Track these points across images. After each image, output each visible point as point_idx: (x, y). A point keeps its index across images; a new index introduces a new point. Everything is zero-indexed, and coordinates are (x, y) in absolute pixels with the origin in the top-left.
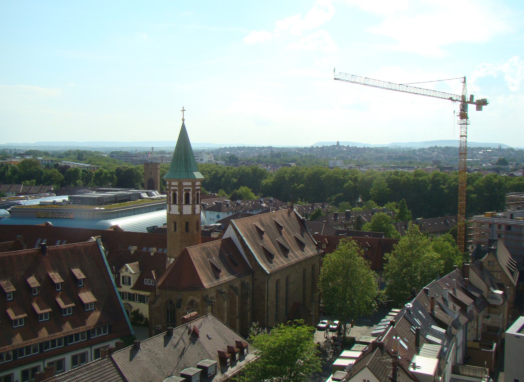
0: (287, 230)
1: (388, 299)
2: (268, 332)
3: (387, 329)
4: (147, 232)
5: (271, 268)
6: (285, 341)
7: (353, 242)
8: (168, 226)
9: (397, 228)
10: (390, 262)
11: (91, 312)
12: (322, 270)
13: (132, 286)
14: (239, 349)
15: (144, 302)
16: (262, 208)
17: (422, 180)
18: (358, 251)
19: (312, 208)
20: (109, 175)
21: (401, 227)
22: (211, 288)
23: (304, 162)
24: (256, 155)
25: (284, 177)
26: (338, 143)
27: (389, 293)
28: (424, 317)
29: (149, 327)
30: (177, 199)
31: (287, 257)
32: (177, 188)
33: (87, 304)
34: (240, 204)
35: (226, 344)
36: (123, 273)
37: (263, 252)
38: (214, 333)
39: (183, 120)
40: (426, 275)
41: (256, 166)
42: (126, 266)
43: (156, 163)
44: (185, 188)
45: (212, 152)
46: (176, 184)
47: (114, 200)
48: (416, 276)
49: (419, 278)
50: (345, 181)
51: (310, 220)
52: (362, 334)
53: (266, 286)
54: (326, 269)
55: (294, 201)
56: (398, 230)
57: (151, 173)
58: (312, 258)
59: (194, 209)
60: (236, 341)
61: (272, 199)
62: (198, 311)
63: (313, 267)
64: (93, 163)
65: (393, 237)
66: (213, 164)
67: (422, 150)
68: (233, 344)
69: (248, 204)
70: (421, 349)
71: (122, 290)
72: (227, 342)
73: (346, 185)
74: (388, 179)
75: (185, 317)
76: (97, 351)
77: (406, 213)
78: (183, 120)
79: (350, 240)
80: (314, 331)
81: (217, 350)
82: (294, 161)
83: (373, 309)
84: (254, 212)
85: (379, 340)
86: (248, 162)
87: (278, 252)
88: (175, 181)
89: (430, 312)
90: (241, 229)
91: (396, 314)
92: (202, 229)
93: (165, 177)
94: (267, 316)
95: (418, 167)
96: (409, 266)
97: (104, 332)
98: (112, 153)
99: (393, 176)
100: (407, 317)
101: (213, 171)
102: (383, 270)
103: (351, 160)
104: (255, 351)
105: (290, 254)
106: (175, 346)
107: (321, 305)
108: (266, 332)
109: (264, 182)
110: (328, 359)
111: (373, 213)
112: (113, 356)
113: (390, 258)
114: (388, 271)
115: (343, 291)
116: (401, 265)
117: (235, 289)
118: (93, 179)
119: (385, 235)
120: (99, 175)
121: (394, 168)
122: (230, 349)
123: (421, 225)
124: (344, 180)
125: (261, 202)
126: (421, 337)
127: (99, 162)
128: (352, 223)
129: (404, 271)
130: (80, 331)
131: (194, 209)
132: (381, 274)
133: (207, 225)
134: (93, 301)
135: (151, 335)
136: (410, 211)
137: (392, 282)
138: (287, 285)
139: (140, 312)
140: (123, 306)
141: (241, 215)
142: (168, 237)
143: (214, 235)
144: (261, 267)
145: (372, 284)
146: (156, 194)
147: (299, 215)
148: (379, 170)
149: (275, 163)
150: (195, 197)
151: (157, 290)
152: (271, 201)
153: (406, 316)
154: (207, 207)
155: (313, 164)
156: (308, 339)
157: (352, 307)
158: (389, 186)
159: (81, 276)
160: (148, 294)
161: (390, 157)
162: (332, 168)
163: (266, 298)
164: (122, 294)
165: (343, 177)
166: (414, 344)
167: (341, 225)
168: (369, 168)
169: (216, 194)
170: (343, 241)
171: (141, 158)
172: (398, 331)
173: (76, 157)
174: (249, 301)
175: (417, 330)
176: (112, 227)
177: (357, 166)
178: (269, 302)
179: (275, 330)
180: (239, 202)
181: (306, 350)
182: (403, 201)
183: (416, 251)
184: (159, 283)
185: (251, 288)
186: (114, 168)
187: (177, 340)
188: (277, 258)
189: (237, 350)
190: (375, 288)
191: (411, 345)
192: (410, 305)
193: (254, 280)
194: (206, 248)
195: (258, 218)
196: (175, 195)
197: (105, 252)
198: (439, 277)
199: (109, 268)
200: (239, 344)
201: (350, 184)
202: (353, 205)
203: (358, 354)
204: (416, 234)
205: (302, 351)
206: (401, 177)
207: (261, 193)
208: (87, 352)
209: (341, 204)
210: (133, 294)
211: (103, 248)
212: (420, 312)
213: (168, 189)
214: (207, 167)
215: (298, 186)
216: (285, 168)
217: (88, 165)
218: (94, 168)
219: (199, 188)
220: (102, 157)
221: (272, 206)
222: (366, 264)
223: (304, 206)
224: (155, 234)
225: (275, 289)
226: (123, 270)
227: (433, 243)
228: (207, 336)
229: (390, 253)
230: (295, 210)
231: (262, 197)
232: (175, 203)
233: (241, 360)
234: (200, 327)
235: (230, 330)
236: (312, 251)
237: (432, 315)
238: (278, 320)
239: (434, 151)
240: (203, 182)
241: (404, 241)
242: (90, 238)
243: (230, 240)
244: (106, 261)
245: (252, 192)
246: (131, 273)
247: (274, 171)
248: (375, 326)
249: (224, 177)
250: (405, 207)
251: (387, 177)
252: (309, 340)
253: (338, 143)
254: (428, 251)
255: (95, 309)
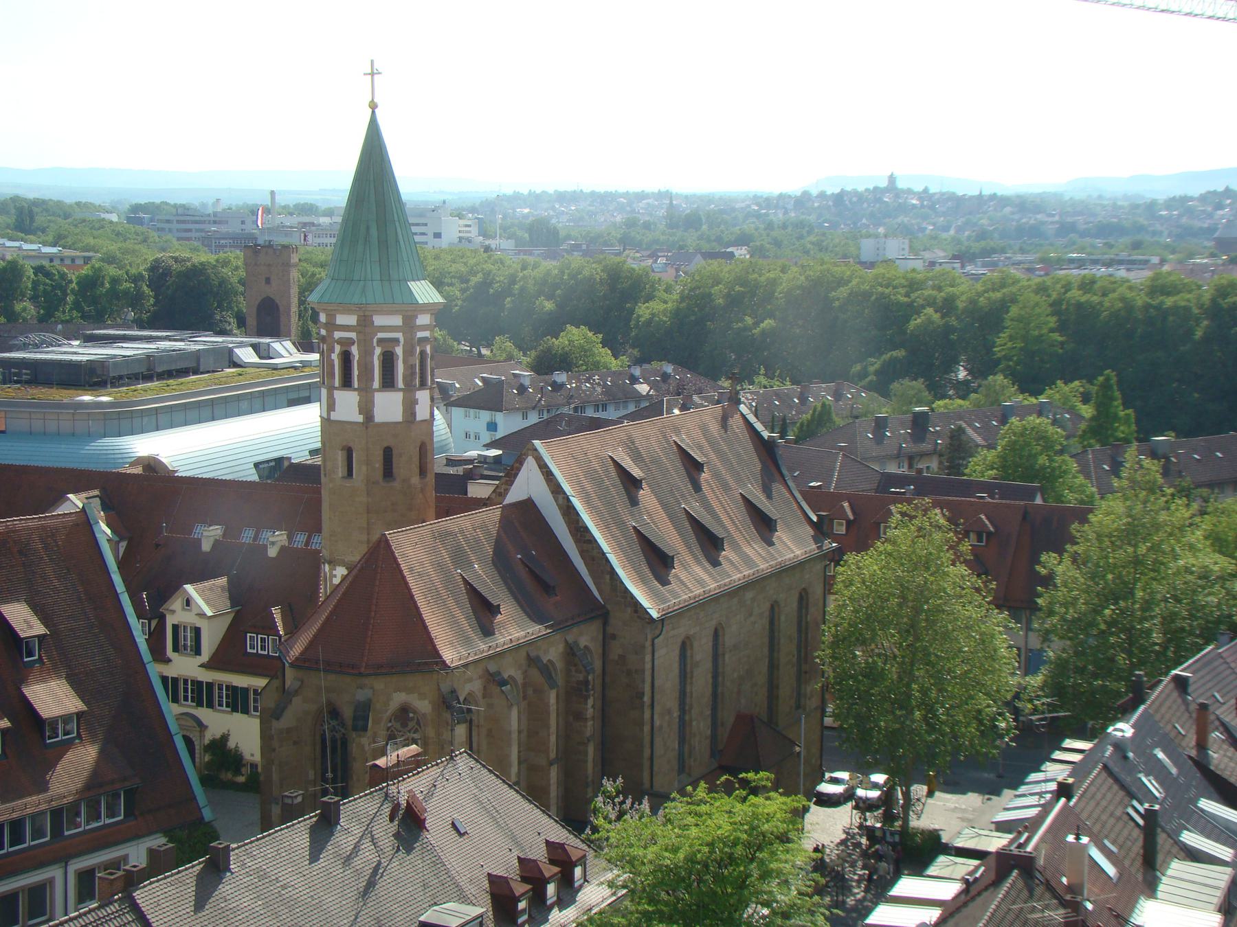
0: (716, 475)
1: (1052, 707)
2: (654, 810)
3: (1046, 809)
4: (255, 478)
5: (664, 601)
6: (711, 844)
7: (938, 516)
8: (324, 461)
9: (1084, 471)
10: (1058, 581)
11: (67, 745)
12: (831, 607)
13: (205, 656)
14: (556, 869)
15: (246, 711)
16: (638, 397)
17: (1175, 309)
18: (951, 547)
19: (803, 400)
20: (126, 285)
21: (1098, 466)
22: (465, 666)
23: (777, 243)
24: (619, 219)
25: (710, 294)
26: (892, 179)
27: (1056, 688)
28: (1174, 771)
29: (263, 798)
30: (356, 372)
31: (715, 563)
32: (353, 335)
33: (54, 722)
34: (562, 385)
35: (516, 853)
36: (176, 615)
37: (637, 547)
38: (479, 817)
39: (373, 106)
40: (1183, 629)
41: (618, 259)
42: (185, 591)
43: (285, 247)
44: (380, 335)
45: (473, 210)
46: (352, 320)
47: (143, 370)
48: (1148, 632)
49: (1157, 637)
50: (913, 309)
51: (796, 442)
52: (962, 819)
53: (648, 658)
54: (845, 606)
55: (743, 376)
56: (1088, 476)
57: (268, 281)
58: (799, 566)
59: (410, 406)
60: (547, 842)
61: (669, 369)
62: (425, 744)
63: (803, 598)
64: (69, 240)
65: (1071, 499)
66: (475, 251)
67: (1180, 203)
68: (539, 853)
69: (591, 387)
70: (1164, 879)
71: (171, 671)
72: (518, 844)
73: (915, 323)
74: (1055, 304)
75: (381, 762)
76: (86, 881)
77: (1116, 417)
78: (373, 106)
79: (925, 511)
80: (806, 809)
81: (487, 870)
82: (743, 240)
83: (1001, 737)
84: (611, 413)
85: (1020, 846)
86: (592, 244)
87: (689, 548)
88: (347, 311)
89: (1193, 753)
90: (563, 472)
91: (1076, 757)
92: (439, 466)
93: (313, 298)
94: (651, 759)
95: (1163, 261)
96: (1125, 599)
97: (111, 814)
98: (136, 208)
99: (1075, 294)
100: (1116, 769)
101: (475, 274)
102: (1035, 608)
103: (935, 238)
104: (610, 876)
105: (727, 553)
106: (348, 860)
107: (828, 721)
108: (648, 810)
109: (644, 311)
110: (850, 901)
111: (1004, 420)
112: (140, 895)
113: (1060, 569)
114: (1051, 613)
115: (900, 678)
116: (1098, 595)
117: (546, 670)
118: (70, 299)
119: (1042, 490)
120: (90, 284)
121: (1080, 263)
122: (530, 872)
123: (1167, 459)
124: (910, 305)
125: (634, 380)
126: (1161, 838)
127: (92, 241)
128: (935, 452)
129: (1107, 612)
130: (29, 811)
131: (410, 406)
132: (1029, 622)
133: (454, 453)
134: (73, 710)
135: (266, 824)
136: (1130, 411)
137: (1064, 650)
138: (716, 656)
139: (231, 744)
140: (173, 726)
141: (569, 423)
142: (325, 494)
143: (478, 490)
144: (632, 597)
145: (997, 659)
146: (286, 352)
147: (759, 426)
148: (1030, 270)
149: (681, 248)
150: (413, 367)
151: (289, 673)
152: (665, 377)
153: (1111, 765)
154: (455, 396)
155: (807, 252)
156: (784, 839)
157: (932, 728)
158: (1062, 328)
159: (31, 627)
160: (261, 682)
161: (1066, 229)
162: (872, 265)
163: (647, 699)
164: (172, 685)
165: (907, 295)
166: (1139, 862)
167: (898, 456)
168: (994, 265)
169: (484, 351)
170: (903, 514)
171: (234, 228)
172: (1084, 816)
173: (11, 220)
174: (590, 707)
175: (1149, 816)
176: (139, 461)
177: (955, 257)
178: (657, 709)
179: (676, 807)
180: (560, 377)
181: (779, 873)
182: (1108, 379)
183: (1149, 549)
184: (296, 650)
185: (598, 664)
186: (142, 259)
187: (352, 840)
188: (685, 566)
189: (550, 870)
190: (1007, 670)
191: (1127, 863)
192: (1124, 729)
193: (607, 639)
194: (450, 534)
195: (623, 435)
196: (346, 358)
197: (114, 545)
198: (1226, 638)
199: (125, 600)
200: (557, 853)
201: (930, 321)
202: (938, 392)
203: (948, 891)
204: (1151, 491)
205: (766, 875)
206: (1104, 295)
207: (633, 347)
208: (51, 881)
209: (895, 386)
210: (210, 685)
211: (108, 531)
212: (1161, 755)
213: (323, 339)
214: (454, 261)
215: (756, 324)
216: (715, 265)
217: (54, 250)
218: (73, 260)
219: (426, 334)
220: (102, 224)
221: (668, 393)
222: (978, 590)
223: (778, 395)
224: (286, 485)
225: (676, 671)
226: (176, 604)
227: (1206, 524)
228: (453, 825)
229: (1060, 551)
230: (743, 408)
231: (638, 362)
232: (347, 383)
233: (562, 903)
234: (429, 795)
235: (527, 806)
236: (798, 541)
237: (1202, 765)
238: (686, 777)
239: (1220, 206)
240: (441, 315)
241: (1110, 513)
242: (60, 498)
243: (528, 506)
244: (117, 579)
245: (604, 344)
246: (202, 615)
247: (677, 276)
248: (1007, 793)
249: (511, 295)
250: (1112, 399)
251: (1054, 296)
252: (789, 841)
253: (892, 179)
254: (1192, 547)
255: (79, 736)
